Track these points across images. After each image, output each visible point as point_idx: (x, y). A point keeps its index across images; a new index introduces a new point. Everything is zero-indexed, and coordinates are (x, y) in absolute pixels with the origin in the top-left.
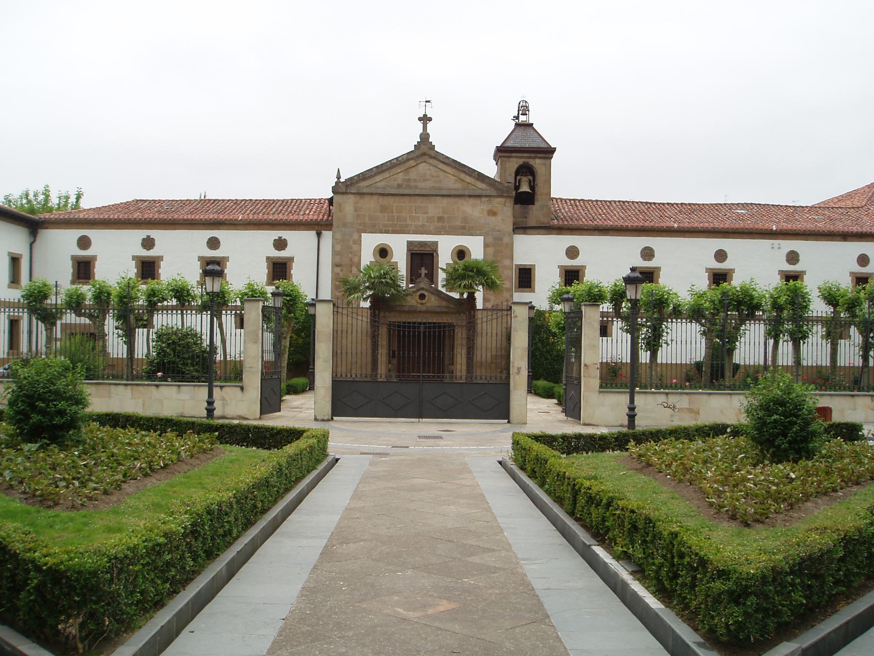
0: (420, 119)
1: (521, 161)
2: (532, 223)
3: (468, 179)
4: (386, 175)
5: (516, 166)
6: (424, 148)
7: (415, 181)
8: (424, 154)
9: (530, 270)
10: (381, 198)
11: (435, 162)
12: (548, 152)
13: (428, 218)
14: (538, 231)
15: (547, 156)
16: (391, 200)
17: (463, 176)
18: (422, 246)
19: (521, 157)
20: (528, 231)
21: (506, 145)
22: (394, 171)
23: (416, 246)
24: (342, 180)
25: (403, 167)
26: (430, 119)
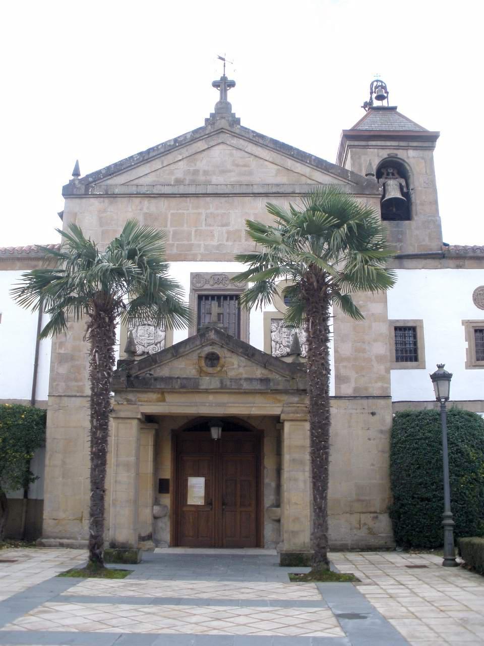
0: (216, 85)
1: (384, 154)
2: (411, 249)
3: (299, 168)
4: (157, 164)
5: (376, 162)
6: (223, 123)
7: (206, 173)
8: (221, 131)
9: (414, 329)
10: (146, 202)
11: (242, 143)
12: (425, 140)
13: (228, 232)
14: (429, 261)
15: (426, 144)
16: (163, 204)
17: (290, 163)
18: (218, 282)
19: (383, 148)
20: (406, 262)
21: (360, 128)
22: (170, 158)
23: (207, 282)
24: (83, 174)
25: (185, 152)
26: (232, 84)
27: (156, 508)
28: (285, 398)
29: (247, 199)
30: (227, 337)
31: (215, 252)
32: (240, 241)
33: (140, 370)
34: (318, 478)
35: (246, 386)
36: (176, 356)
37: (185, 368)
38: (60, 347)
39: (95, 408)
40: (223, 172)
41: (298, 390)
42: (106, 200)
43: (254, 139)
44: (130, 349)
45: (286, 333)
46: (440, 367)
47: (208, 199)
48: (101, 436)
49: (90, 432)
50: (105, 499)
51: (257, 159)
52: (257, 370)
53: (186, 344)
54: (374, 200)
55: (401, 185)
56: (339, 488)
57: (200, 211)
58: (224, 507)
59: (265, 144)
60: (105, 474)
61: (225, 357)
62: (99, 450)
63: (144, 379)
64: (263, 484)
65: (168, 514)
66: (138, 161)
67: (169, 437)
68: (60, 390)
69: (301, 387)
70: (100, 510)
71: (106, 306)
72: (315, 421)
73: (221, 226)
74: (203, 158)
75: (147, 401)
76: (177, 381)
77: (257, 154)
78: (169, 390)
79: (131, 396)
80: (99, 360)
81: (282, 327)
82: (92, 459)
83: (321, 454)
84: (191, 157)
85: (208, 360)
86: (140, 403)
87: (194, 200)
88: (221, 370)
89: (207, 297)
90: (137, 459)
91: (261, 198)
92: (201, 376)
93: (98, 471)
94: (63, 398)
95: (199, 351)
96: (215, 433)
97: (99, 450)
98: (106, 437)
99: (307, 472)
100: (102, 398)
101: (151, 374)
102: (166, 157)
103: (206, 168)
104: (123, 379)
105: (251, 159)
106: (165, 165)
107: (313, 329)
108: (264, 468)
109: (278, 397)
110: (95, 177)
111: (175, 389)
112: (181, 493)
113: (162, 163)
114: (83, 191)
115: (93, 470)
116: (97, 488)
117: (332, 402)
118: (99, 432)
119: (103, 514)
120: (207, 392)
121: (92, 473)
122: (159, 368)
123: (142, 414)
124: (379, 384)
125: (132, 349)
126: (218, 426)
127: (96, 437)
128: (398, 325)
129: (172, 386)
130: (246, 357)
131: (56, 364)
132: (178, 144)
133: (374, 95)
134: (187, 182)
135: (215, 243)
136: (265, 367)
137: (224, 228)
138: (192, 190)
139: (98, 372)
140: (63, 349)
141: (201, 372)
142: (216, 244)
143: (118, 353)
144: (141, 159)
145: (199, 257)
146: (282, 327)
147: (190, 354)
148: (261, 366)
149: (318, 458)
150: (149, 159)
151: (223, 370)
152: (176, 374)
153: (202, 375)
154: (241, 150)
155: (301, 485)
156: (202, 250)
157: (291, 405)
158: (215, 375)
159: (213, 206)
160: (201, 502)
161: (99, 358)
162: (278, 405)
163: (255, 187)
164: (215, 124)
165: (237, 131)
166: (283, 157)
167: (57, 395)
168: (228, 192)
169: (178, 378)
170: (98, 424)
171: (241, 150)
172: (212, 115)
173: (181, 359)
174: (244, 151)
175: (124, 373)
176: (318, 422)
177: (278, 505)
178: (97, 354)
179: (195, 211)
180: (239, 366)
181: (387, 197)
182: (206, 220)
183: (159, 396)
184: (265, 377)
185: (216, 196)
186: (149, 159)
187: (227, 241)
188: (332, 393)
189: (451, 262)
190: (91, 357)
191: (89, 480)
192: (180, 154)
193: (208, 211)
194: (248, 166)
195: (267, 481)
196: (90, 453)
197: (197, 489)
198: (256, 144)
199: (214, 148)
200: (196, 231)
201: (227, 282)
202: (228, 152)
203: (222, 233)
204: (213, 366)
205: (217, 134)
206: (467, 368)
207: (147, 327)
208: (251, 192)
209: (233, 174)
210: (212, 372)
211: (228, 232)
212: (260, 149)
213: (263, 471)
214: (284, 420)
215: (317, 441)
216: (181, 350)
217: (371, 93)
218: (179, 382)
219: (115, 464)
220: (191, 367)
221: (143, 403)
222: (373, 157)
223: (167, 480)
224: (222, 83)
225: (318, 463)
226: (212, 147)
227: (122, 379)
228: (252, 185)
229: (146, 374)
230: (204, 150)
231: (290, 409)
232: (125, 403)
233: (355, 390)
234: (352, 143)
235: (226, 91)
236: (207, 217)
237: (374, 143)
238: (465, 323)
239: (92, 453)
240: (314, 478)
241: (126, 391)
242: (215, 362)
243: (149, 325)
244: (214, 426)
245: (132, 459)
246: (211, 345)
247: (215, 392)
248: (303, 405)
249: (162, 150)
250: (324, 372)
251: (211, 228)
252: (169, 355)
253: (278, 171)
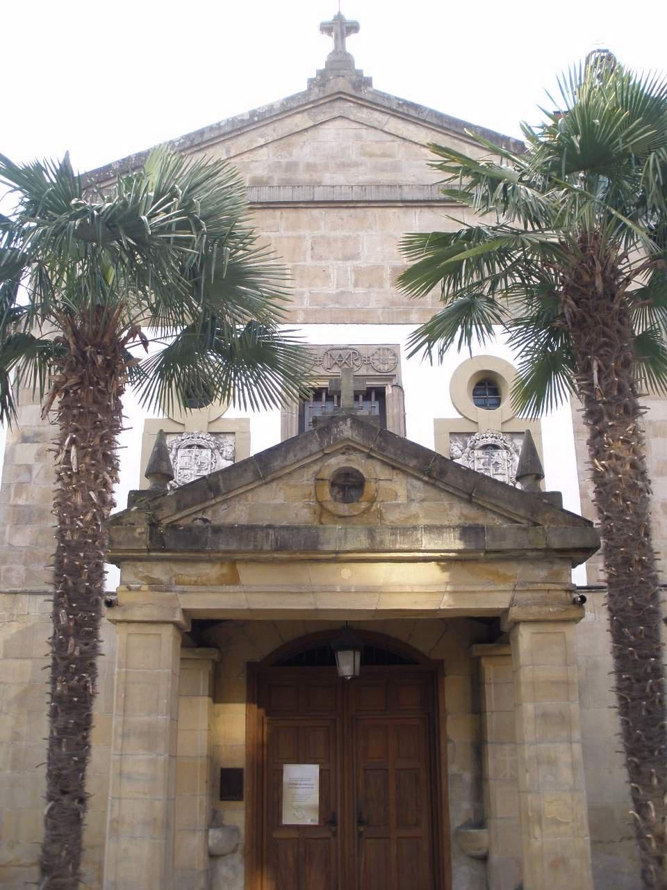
0: (326, 28)
6: (342, 84)
7: (310, 167)
8: (339, 97)
11: (377, 117)
13: (357, 271)
25: (271, 133)
26: (353, 28)
27: (215, 834)
28: (517, 571)
29: (391, 212)
30: (380, 435)
31: (331, 306)
32: (381, 286)
33: (179, 509)
34: (646, 754)
36: (264, 478)
37: (284, 503)
38: (19, 492)
39: (66, 580)
40: (344, 166)
41: (548, 550)
43: (400, 110)
44: (159, 467)
45: (482, 461)
47: (316, 212)
48: (77, 653)
49: (50, 644)
50: (85, 821)
51: (407, 144)
52: (451, 508)
53: (287, 452)
57: (302, 232)
58: (362, 829)
59: (421, 117)
60: (88, 752)
61: (377, 480)
62: (71, 689)
63: (189, 529)
64: (447, 776)
65: (241, 847)
66: (182, 148)
67: (243, 679)
68: (15, 581)
70: (69, 853)
71: (100, 335)
72: (627, 605)
73: (342, 260)
74: (304, 142)
75: (196, 583)
76: (267, 535)
77: (405, 135)
78: (249, 556)
79: (159, 572)
80: (78, 463)
81: (473, 448)
82: (54, 714)
83: (648, 690)
84: (282, 142)
85: (336, 489)
86: (179, 588)
87: (289, 214)
88: (368, 509)
90: (172, 719)
91: (418, 210)
92: (322, 523)
93: (67, 745)
94: (18, 596)
95: (316, 468)
96: (347, 665)
97: (71, 689)
98: (92, 657)
99: (578, 742)
100: (82, 555)
101: (205, 521)
102: (234, 141)
103: (311, 160)
104: (141, 529)
105: (396, 144)
106: (232, 155)
107: (605, 383)
108: (447, 740)
109: (502, 568)
110: (100, 176)
111: (261, 551)
115: (55, 742)
116: (64, 793)
118: (72, 641)
119: (76, 865)
121: (51, 750)
122: (225, 506)
123: (185, 612)
125: (164, 468)
126: (354, 648)
127: (64, 655)
129: (255, 546)
130: (426, 479)
131: (8, 528)
134: (275, 183)
135: (332, 290)
136: (469, 501)
137: (349, 265)
138: (286, 195)
139: (75, 490)
140: (24, 496)
141: (321, 515)
142: (334, 292)
143: (130, 476)
144: (188, 143)
146: (473, 448)
147: (295, 475)
148: (461, 499)
149: (641, 698)
150: (202, 143)
151: (374, 508)
152: (264, 519)
153: (323, 520)
154: (375, 128)
155: (566, 775)
156: (306, 304)
157: (531, 587)
158: (355, 520)
159: (326, 221)
160: (310, 818)
161: (78, 458)
162: (501, 587)
163: (406, 189)
164: (327, 86)
165: (369, 97)
166: (456, 141)
167: (7, 590)
168: (355, 198)
169: (270, 527)
170: (71, 624)
171: (375, 128)
173: (274, 484)
174: (382, 130)
175: (144, 516)
176: (634, 608)
177: (481, 823)
178: (73, 450)
179: (290, 233)
180: (410, 500)
182: (312, 249)
183: (225, 570)
184: (471, 522)
185: (333, 205)
186: (202, 143)
187: (356, 285)
190: (61, 457)
191: (43, 770)
192: (262, 136)
193: (316, 233)
194: (390, 156)
196: (48, 698)
197: (302, 788)
198: (403, 119)
199: (326, 126)
201: (358, 363)
202: (351, 132)
203: (346, 271)
204: (346, 500)
205: (330, 101)
207: (195, 451)
208: (399, 199)
209: (362, 169)
210: (347, 514)
211: (357, 271)
212: (411, 127)
213: (446, 747)
214: (517, 623)
215: (636, 657)
216: (277, 464)
218: (272, 537)
219: (120, 730)
220: (299, 504)
221: (186, 588)
224: (337, 23)
225: (644, 713)
226: (321, 124)
227: (138, 530)
228: (400, 186)
229: (196, 519)
230: (306, 130)
231: (529, 595)
232: (145, 588)
235: (343, 37)
239: (56, 697)
240: (630, 752)
241: (148, 560)
242: (353, 493)
243: (200, 447)
244: (344, 648)
245: (162, 719)
246: (343, 453)
248: (558, 587)
249: (228, 129)
250: (640, 484)
251: (323, 263)
252: (249, 476)
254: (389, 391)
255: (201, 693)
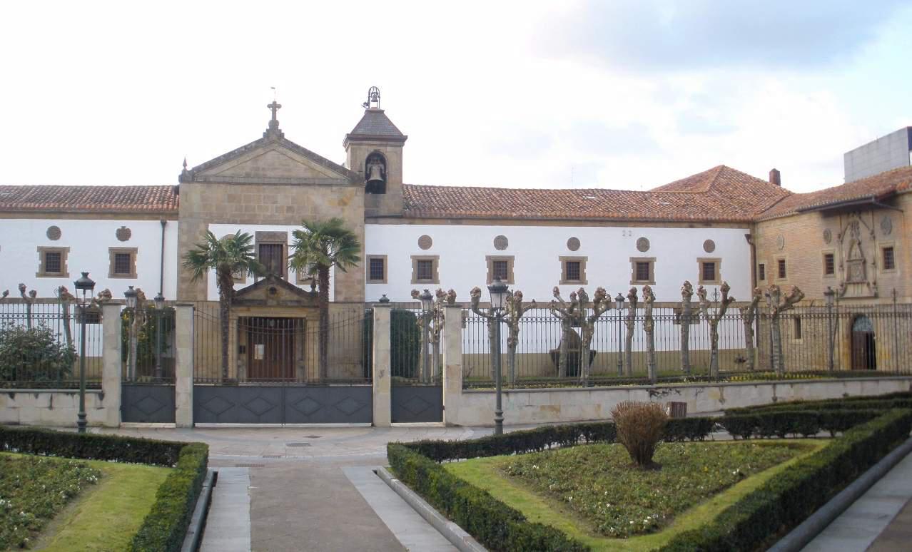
0: (269, 106)
1: (372, 149)
3: (319, 167)
4: (234, 163)
6: (274, 137)
7: (263, 169)
10: (229, 187)
12: (400, 140)
13: (276, 208)
15: (398, 143)
16: (239, 188)
17: (313, 164)
23: (265, 237)
24: (189, 168)
25: (252, 155)
26: (279, 107)
27: (239, 362)
28: (309, 310)
35: (289, 304)
37: (260, 294)
42: (205, 185)
46: (384, 296)
54: (360, 189)
55: (381, 169)
56: (333, 351)
69: (316, 304)
89: (264, 245)
112: (251, 353)
113: (238, 161)
114: (191, 179)
117: (330, 305)
120: (270, 306)
124: (358, 296)
128: (373, 258)
132: (247, 149)
133: (371, 99)
137: (275, 205)
138: (255, 180)
145: (260, 222)
152: (256, 298)
159: (269, 191)
160: (261, 358)
172: (267, 130)
181: (372, 179)
188: (331, 298)
189: (407, 221)
195: (297, 346)
197: (260, 350)
200: (258, 206)
206: (412, 283)
211: (276, 208)
217: (369, 97)
222: (366, 150)
223: (245, 347)
233: (346, 298)
234: (352, 142)
236: (264, 198)
237: (364, 142)
238: (412, 257)
247: (274, 307)
253: (306, 170)
254: (284, 246)
255: (678, 405)
